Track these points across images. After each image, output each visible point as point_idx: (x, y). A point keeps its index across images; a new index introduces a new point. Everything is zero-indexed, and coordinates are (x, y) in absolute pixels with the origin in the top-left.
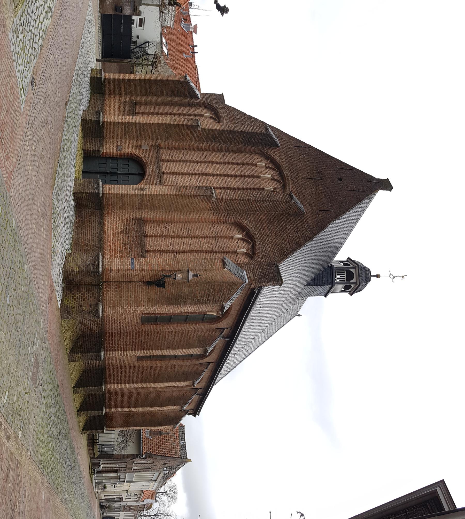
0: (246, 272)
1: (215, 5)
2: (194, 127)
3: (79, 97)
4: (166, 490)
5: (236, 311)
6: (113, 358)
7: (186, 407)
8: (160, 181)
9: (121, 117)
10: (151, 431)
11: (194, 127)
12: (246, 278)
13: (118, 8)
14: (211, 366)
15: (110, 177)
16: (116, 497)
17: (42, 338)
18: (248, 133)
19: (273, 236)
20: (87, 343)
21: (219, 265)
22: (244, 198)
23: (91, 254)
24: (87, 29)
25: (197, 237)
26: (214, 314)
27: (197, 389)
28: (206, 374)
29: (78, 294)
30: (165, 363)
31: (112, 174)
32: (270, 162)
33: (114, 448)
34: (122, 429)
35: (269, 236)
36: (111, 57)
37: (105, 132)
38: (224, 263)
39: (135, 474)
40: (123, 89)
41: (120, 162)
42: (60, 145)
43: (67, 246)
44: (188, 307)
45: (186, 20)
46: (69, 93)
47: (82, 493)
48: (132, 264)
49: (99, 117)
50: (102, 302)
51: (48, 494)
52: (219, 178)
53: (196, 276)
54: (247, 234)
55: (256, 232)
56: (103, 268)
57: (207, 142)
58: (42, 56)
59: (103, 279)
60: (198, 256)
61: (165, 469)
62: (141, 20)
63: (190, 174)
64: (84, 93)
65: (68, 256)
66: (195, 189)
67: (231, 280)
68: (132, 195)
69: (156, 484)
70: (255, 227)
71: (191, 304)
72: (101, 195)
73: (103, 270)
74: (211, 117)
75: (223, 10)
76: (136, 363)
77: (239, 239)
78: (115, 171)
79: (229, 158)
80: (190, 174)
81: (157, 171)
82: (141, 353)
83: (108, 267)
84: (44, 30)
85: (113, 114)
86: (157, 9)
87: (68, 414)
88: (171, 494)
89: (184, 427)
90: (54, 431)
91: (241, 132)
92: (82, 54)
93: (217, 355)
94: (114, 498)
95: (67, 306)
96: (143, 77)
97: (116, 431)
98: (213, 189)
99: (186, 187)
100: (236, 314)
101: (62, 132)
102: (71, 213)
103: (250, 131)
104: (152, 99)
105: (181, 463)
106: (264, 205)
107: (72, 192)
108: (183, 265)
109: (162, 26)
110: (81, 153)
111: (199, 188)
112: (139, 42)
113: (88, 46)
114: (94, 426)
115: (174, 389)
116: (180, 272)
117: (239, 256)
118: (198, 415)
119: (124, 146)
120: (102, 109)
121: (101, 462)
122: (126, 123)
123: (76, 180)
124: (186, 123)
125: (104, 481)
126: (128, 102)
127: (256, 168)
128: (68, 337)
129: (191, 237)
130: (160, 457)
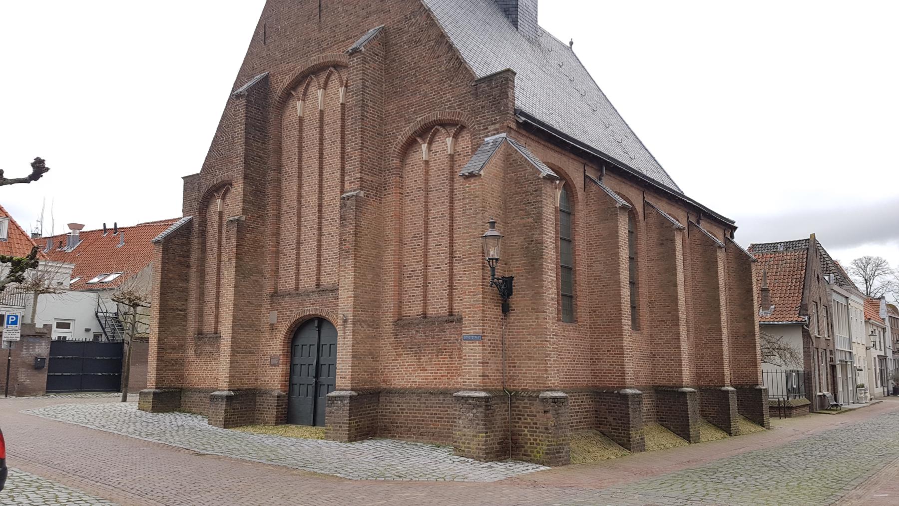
0: (487, 136)
1: (33, 182)
2: (241, 227)
3: (187, 432)
4: (862, 280)
5: (556, 155)
6: (636, 374)
7: (720, 242)
8: (332, 291)
9: (222, 358)
10: (761, 306)
11: (241, 227)
12: (497, 136)
13: (38, 365)
14: (649, 199)
15: (323, 378)
16: (878, 368)
17: (604, 499)
18: (247, 132)
19: (425, 88)
20: (611, 419)
21: (474, 184)
22: (359, 141)
24: (70, 418)
25: (426, 223)
26: (559, 193)
27: (690, 224)
28: (664, 208)
29: (526, 435)
30: (643, 278)
31: (317, 376)
32: (295, 91)
33: (793, 371)
34: (759, 357)
35: (425, 95)
36: (120, 376)
37: (246, 387)
38: (471, 175)
39: (836, 333)
40: (174, 356)
41: (297, 360)
42: (267, 465)
43: (442, 454)
44: (545, 237)
45: (61, 242)
46: (178, 449)
47: (873, 427)
48: (472, 339)
49: (221, 397)
50: (539, 391)
51: (878, 487)
52: (325, 185)
53: (493, 224)
54: (420, 136)
55: (419, 119)
57: (264, 206)
58: (114, 496)
59: (499, 390)
60: (459, 221)
61: (827, 278)
62: (59, 326)
63: (320, 234)
64: (180, 424)
65: (459, 451)
66: (345, 226)
67: (500, 163)
68: (354, 339)
69: (852, 297)
70: (408, 121)
71: (542, 232)
72: (354, 393)
73: (484, 390)
74: (223, 198)
75: (39, 168)
76: (645, 332)
77: (429, 150)
78: (312, 371)
79: (290, 167)
80: (320, 234)
81: (314, 297)
82: (627, 323)
83: (479, 381)
84: (69, 494)
85: (215, 373)
86: (41, 297)
87: (736, 452)
88: (871, 268)
89: (753, 245)
90: (765, 477)
91: (247, 144)
92: (113, 427)
93: (631, 189)
94: (881, 370)
95: (547, 454)
96: (156, 321)
97: (763, 367)
98: (345, 195)
99: (342, 242)
100: (560, 156)
101: (245, 461)
102: (383, 446)
103: (243, 127)
104: (192, 307)
105: (817, 250)
106: (371, 104)
107: (349, 444)
108: (474, 245)
109: (71, 290)
110: (281, 429)
111: (342, 218)
112: (96, 328)
113: (100, 417)
114: (754, 406)
115: (688, 261)
116: (485, 248)
117: (459, 149)
118: (734, 222)
119: (271, 353)
120: (207, 391)
121: (819, 394)
122: (232, 350)
123: (327, 437)
124: (233, 241)
125: (851, 388)
126: (197, 346)
127: (306, 119)
128: (602, 453)
129: (427, 232)
130: (806, 292)
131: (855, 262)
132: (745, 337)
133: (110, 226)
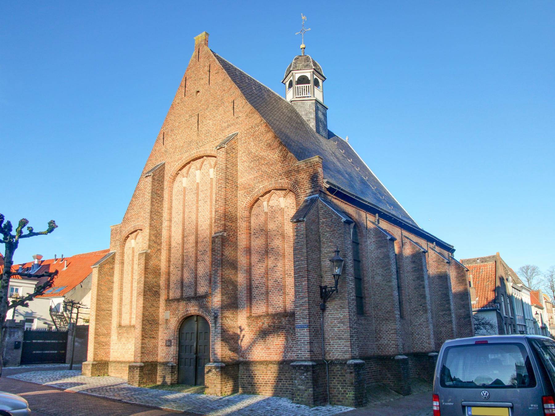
12: (313, 196)
23: (292, 374)
48: (302, 327)
55: (261, 186)
56: (309, 361)
83: (307, 355)
131: (521, 269)
132: (465, 318)
133: (59, 257)
